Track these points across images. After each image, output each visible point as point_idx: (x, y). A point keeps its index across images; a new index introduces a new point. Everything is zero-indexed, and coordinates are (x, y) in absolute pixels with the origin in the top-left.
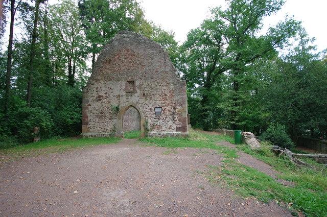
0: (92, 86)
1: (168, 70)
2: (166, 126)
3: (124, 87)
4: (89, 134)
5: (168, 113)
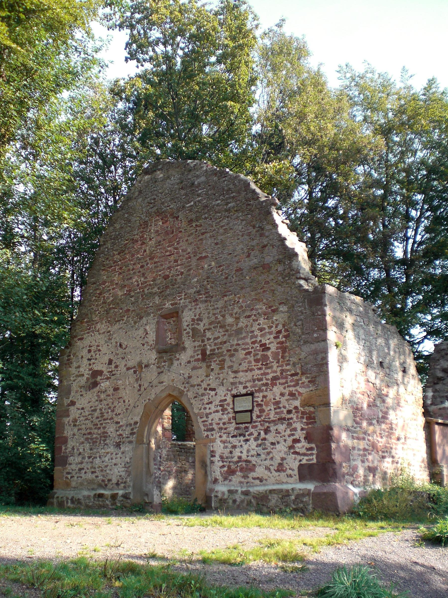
0: (79, 343)
1: (268, 259)
2: (268, 463)
3: (152, 337)
4: (70, 494)
5: (272, 413)
